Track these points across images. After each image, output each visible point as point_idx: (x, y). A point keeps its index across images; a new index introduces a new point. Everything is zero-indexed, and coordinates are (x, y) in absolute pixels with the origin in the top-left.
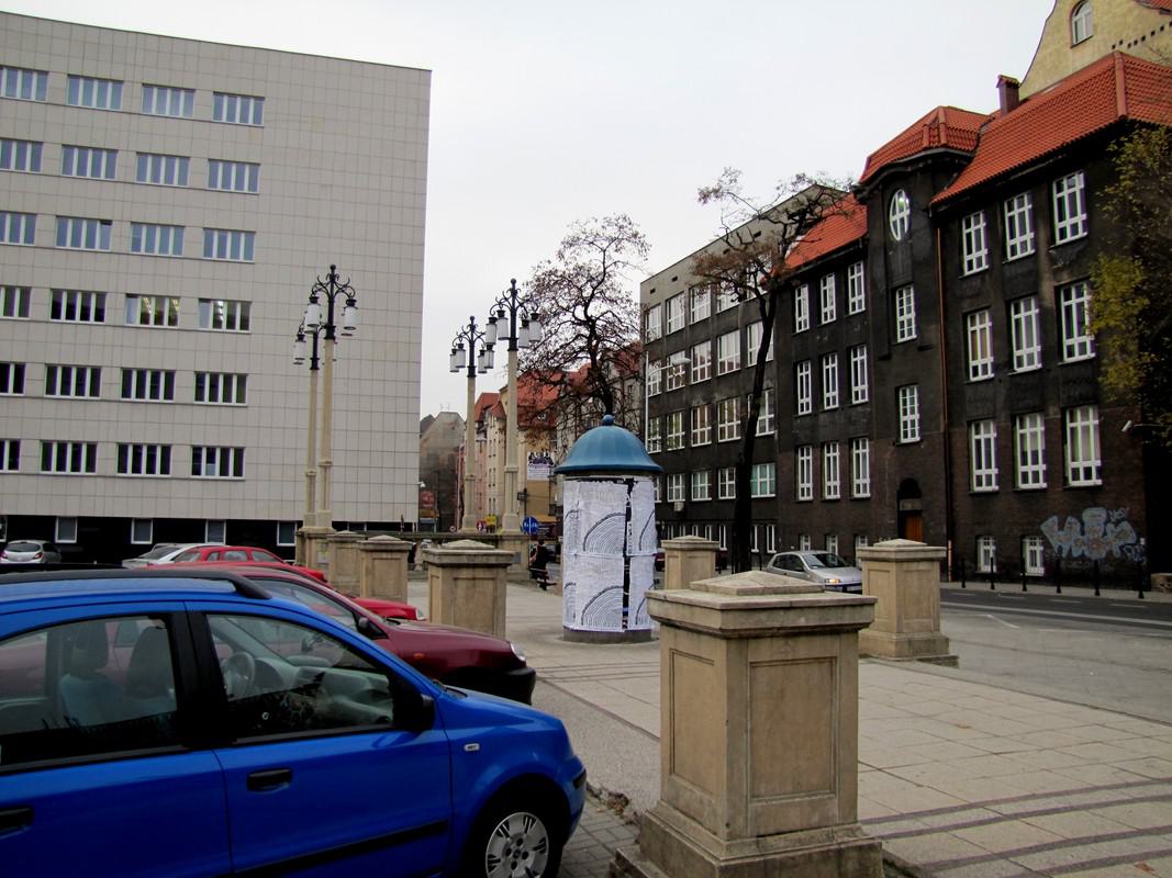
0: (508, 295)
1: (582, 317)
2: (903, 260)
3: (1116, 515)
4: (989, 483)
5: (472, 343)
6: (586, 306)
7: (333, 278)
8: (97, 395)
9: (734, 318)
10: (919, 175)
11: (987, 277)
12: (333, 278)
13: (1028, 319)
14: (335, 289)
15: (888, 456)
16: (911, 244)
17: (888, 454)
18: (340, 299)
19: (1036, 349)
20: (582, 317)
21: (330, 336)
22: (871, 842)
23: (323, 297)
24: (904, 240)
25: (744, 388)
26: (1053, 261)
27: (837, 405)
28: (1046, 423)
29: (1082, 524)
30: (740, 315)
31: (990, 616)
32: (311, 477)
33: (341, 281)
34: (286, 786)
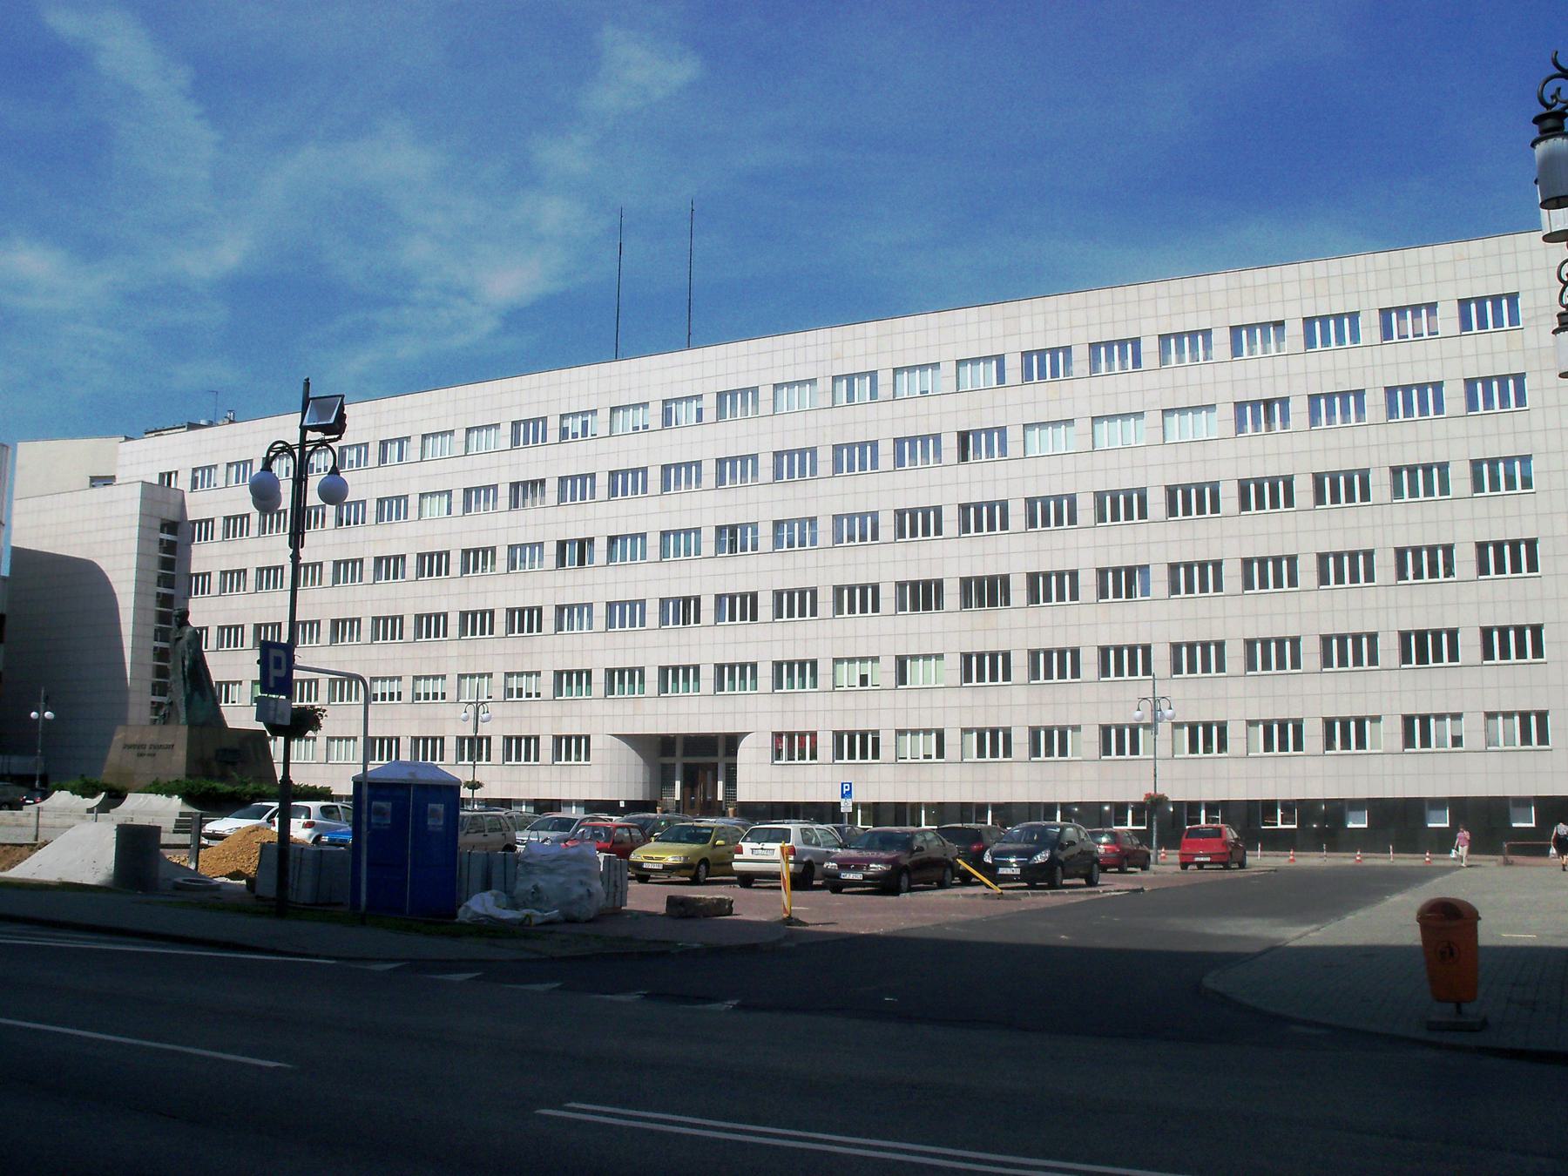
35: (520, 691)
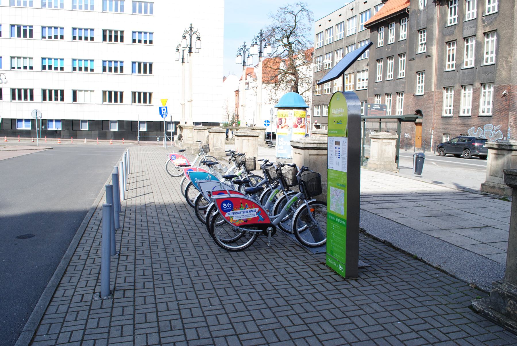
0: (243, 47)
1: (286, 43)
2: (423, 18)
3: (496, 128)
4: (450, 113)
5: (244, 52)
6: (288, 38)
7: (191, 29)
8: (123, 12)
9: (353, 39)
10: (168, 131)
11: (457, 27)
12: (191, 29)
13: (472, 45)
14: (192, 33)
15: (411, 100)
16: (427, 12)
17: (411, 99)
18: (194, 37)
19: (473, 59)
20: (286, 43)
21: (190, 52)
22: (252, 209)
23: (188, 36)
24: (424, 10)
25: (356, 69)
26: (484, 22)
27: (392, 78)
28: (474, 89)
29: (484, 130)
30: (356, 38)
31: (434, 163)
32: (183, 105)
33: (194, 30)
34: (474, 303)
35: (86, 69)
